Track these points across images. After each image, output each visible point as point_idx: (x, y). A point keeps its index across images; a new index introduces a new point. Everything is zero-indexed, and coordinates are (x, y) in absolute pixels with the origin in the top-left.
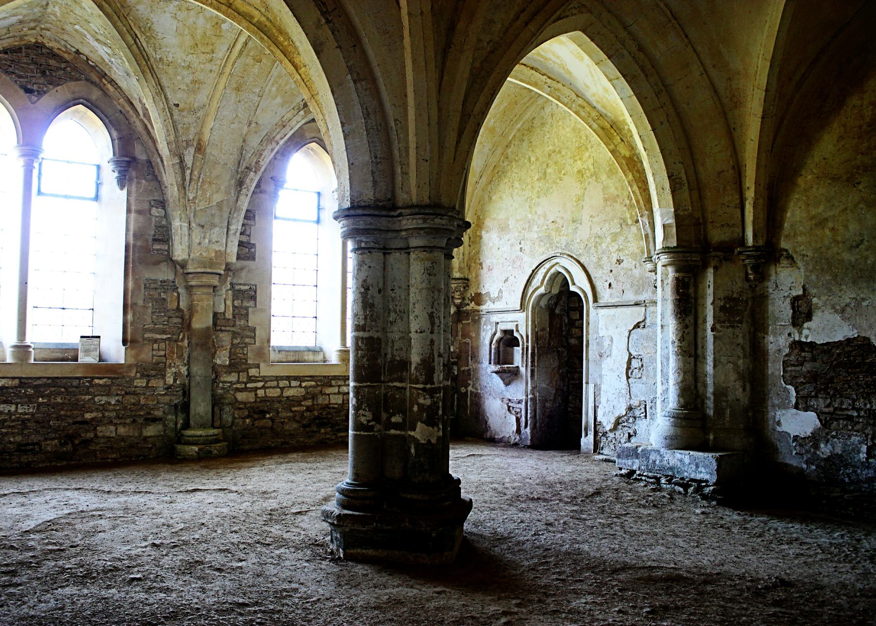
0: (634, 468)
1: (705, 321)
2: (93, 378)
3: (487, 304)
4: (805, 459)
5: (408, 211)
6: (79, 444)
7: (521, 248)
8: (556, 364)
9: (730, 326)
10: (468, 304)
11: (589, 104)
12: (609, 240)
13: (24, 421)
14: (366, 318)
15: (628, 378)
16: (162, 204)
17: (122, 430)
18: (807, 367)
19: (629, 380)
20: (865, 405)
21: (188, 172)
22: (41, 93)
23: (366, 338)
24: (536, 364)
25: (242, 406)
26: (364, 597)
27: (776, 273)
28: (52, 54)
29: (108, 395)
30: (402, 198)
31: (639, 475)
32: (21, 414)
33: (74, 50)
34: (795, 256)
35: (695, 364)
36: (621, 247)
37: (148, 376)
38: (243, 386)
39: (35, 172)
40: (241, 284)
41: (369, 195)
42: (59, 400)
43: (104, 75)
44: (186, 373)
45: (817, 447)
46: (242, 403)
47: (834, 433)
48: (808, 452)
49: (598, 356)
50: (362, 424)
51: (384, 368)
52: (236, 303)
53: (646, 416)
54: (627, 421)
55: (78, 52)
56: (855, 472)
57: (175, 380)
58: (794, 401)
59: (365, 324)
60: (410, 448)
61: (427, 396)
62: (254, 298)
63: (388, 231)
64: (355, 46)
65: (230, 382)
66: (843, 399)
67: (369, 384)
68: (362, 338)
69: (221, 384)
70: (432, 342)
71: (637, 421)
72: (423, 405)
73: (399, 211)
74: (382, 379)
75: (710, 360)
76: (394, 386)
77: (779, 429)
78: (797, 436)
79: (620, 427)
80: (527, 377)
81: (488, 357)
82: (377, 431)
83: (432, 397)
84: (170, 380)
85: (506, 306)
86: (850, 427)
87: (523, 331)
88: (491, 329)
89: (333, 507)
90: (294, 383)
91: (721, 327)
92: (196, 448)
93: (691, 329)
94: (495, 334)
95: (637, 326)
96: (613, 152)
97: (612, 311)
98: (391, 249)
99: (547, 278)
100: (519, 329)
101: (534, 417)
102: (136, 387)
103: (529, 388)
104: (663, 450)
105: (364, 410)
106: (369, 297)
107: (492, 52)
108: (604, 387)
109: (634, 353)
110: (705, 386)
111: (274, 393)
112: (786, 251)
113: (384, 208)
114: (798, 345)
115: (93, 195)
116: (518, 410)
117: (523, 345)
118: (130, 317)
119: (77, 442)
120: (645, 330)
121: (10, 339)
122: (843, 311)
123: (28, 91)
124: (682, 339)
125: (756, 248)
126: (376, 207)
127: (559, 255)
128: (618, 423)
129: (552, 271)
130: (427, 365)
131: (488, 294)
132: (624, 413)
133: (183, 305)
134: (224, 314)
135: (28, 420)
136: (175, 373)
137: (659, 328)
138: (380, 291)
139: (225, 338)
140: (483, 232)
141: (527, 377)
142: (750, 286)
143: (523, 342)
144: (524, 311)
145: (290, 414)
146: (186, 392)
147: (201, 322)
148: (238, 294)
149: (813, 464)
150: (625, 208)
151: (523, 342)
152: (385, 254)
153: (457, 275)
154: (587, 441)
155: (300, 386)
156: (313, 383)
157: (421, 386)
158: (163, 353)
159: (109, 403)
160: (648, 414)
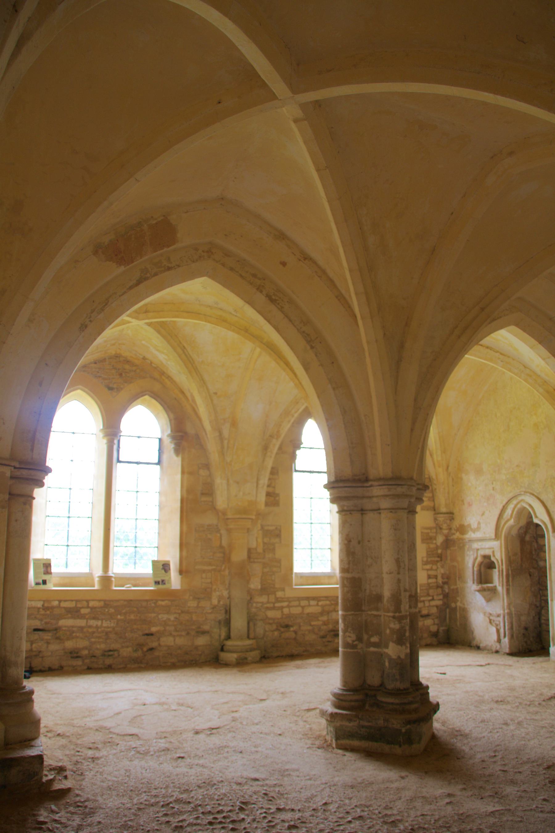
2: (157, 601)
5: (376, 483)
6: (147, 651)
10: (454, 534)
13: (107, 633)
14: (349, 563)
16: (207, 466)
17: (180, 641)
21: (226, 442)
22: (119, 389)
24: (511, 584)
25: (271, 621)
26: (344, 777)
28: (127, 362)
29: (168, 613)
30: (373, 473)
32: (105, 627)
33: (142, 357)
37: (199, 599)
38: (271, 605)
39: (115, 447)
40: (268, 525)
41: (348, 472)
42: (132, 617)
43: (163, 373)
44: (227, 596)
46: (271, 619)
50: (348, 643)
52: (266, 540)
55: (144, 358)
57: (219, 601)
60: (385, 661)
61: (397, 622)
62: (279, 536)
64: (333, 363)
65: (262, 603)
67: (353, 612)
68: (347, 578)
69: (254, 605)
70: (399, 581)
76: (372, 614)
81: (471, 577)
83: (400, 622)
84: (215, 601)
88: (473, 554)
89: (330, 708)
90: (313, 603)
92: (235, 655)
98: (366, 510)
99: (515, 513)
101: (511, 628)
102: (189, 607)
103: (506, 604)
105: (350, 632)
111: (296, 611)
113: (359, 480)
115: (157, 461)
116: (498, 623)
118: (184, 553)
119: (145, 649)
121: (98, 572)
123: (111, 389)
126: (354, 481)
129: (519, 506)
130: (396, 600)
131: (469, 526)
133: (224, 543)
134: (256, 549)
135: (110, 632)
136: (219, 596)
138: (359, 543)
139: (257, 568)
140: (463, 475)
144: (498, 540)
145: (310, 628)
146: (228, 611)
147: (240, 555)
148: (266, 533)
152: (362, 514)
153: (443, 510)
155: (317, 605)
156: (328, 602)
158: (209, 581)
159: (169, 620)
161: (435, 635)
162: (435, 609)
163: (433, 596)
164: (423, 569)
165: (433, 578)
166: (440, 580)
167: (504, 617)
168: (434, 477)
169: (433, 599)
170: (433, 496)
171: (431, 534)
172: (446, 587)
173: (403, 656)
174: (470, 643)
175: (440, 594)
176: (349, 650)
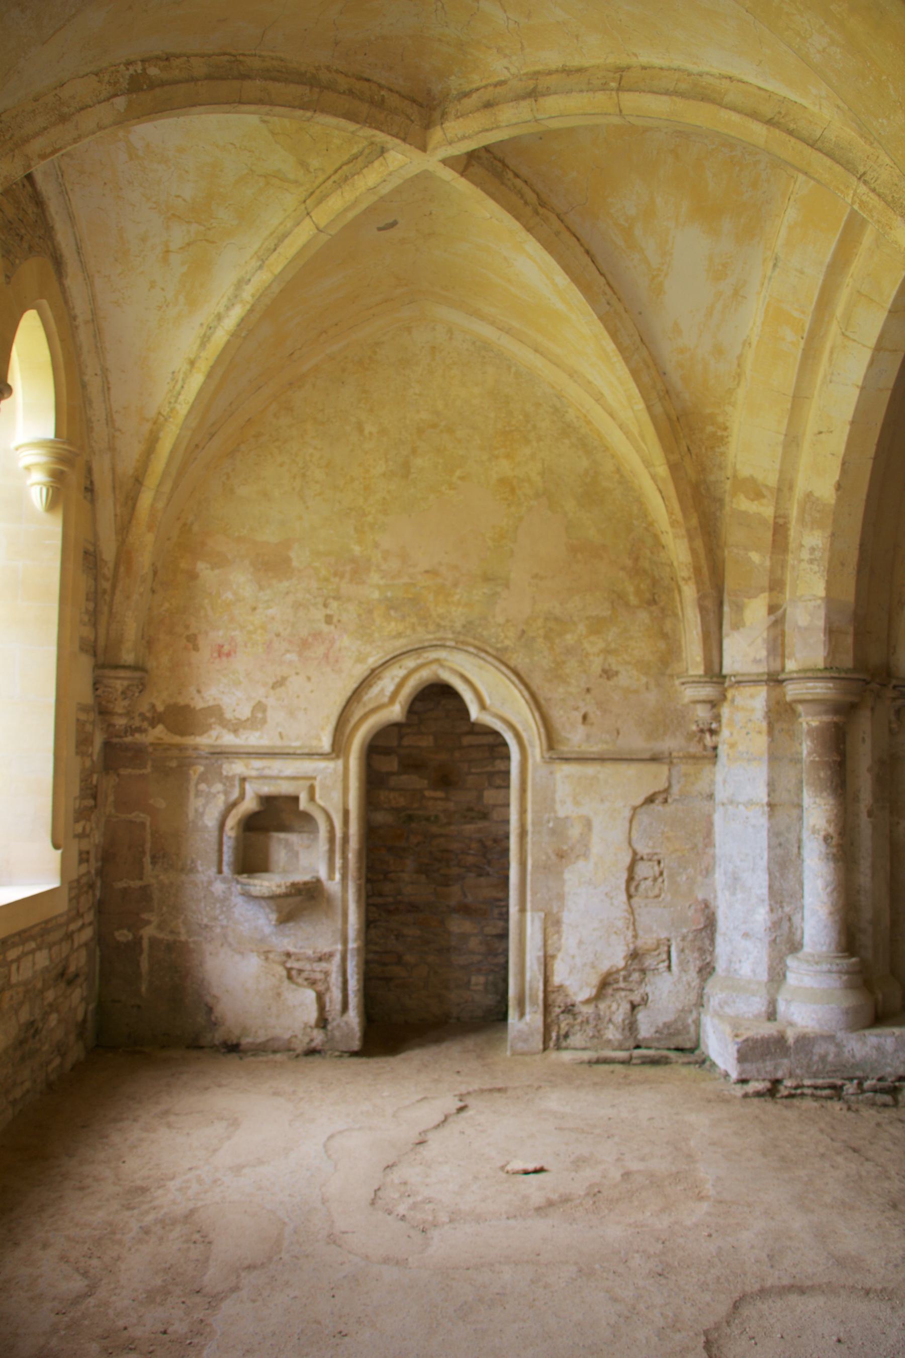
0: (779, 1075)
3: (214, 733)
12: (582, 628)
15: (630, 897)
36: (613, 646)
49: (553, 857)
53: (669, 967)
54: (625, 979)
79: (610, 991)
85: (278, 743)
88: (226, 793)
97: (590, 770)
104: (840, 1035)
108: (568, 917)
109: (643, 849)
120: (670, 808)
128: (605, 984)
132: (621, 964)
144: (338, 757)
150: (622, 574)
167: (344, 959)
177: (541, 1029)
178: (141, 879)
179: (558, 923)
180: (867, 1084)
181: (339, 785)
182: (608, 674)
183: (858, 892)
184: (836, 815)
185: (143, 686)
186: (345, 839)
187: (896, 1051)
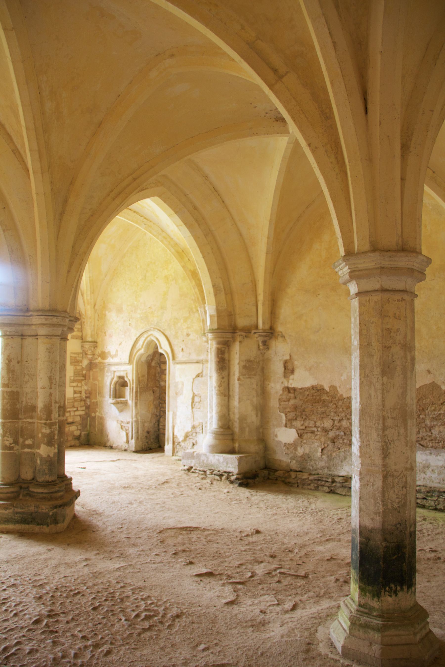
0: (192, 465)
1: (234, 375)
3: (109, 359)
4: (290, 457)
7: (130, 324)
8: (152, 398)
9: (249, 378)
10: (97, 359)
11: (170, 237)
12: (182, 321)
14: (9, 380)
15: (192, 408)
18: (292, 402)
19: (194, 409)
20: (321, 424)
23: (9, 392)
24: (138, 398)
27: (275, 345)
31: (195, 470)
34: (286, 336)
35: (228, 401)
45: (296, 449)
47: (305, 441)
48: (292, 452)
50: (6, 446)
51: (21, 410)
53: (203, 432)
54: (192, 435)
56: (316, 463)
58: (284, 422)
59: (9, 383)
60: (37, 460)
61: (47, 428)
63: (24, 325)
66: (310, 421)
67: (11, 420)
68: (7, 392)
70: (51, 394)
71: (198, 435)
72: (45, 433)
73: (30, 313)
74: (20, 417)
75: (236, 398)
76: (27, 422)
77: (276, 439)
78: (286, 443)
79: (188, 439)
80: (132, 407)
81: (109, 393)
82: (16, 450)
83: (50, 428)
86: (313, 438)
87: (130, 377)
88: (111, 375)
91: (244, 378)
93: (226, 379)
94: (113, 379)
95: (198, 376)
96: (183, 267)
97: (183, 366)
98: (26, 336)
99: (145, 344)
100: (128, 375)
101: (137, 432)
103: (134, 414)
104: (208, 454)
105: (8, 437)
106: (11, 366)
107: (92, 216)
108: (178, 414)
109: (196, 393)
110: (234, 414)
112: (281, 332)
114: (288, 390)
116: (127, 428)
117: (130, 386)
122: (310, 369)
124: (220, 386)
125: (264, 331)
127: (152, 329)
128: (187, 436)
129: (148, 339)
130: (48, 410)
131: (109, 352)
132: (190, 430)
137: (209, 378)
138: (18, 362)
140: (107, 312)
141: (132, 407)
142: (261, 353)
143: (130, 384)
144: (131, 364)
149: (294, 459)
151: (130, 384)
152: (22, 339)
153: (89, 339)
154: (168, 447)
157: (43, 422)
160: (204, 431)
161: (78, 438)
162: (79, 417)
163: (77, 408)
164: (70, 386)
165: (78, 393)
166: (84, 395)
167: (132, 424)
168: (83, 313)
169: (77, 410)
170: (82, 328)
171: (78, 358)
172: (88, 400)
173: (52, 455)
174: (105, 444)
175: (83, 406)
176: (6, 451)
177: (172, 449)
178: (96, 399)
179: (176, 415)
180: (215, 472)
181: (131, 373)
182: (188, 335)
183: (234, 408)
184: (217, 380)
185: (96, 347)
186: (133, 388)
187: (223, 462)
